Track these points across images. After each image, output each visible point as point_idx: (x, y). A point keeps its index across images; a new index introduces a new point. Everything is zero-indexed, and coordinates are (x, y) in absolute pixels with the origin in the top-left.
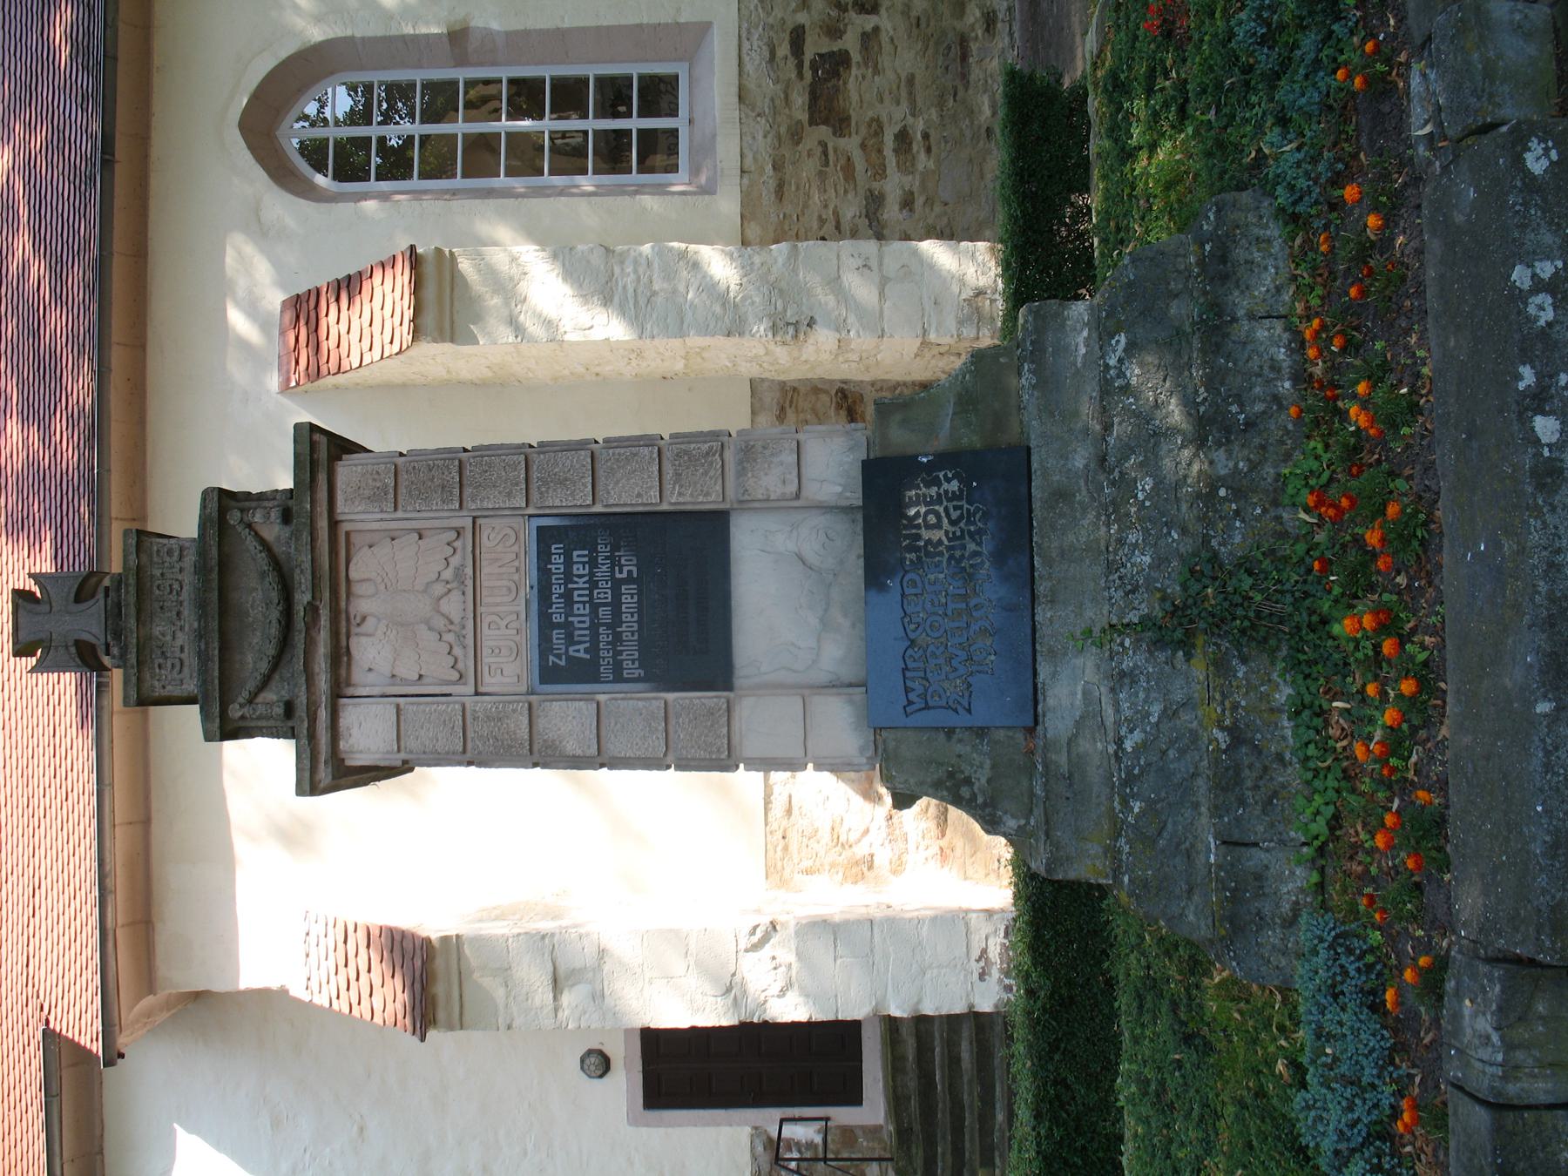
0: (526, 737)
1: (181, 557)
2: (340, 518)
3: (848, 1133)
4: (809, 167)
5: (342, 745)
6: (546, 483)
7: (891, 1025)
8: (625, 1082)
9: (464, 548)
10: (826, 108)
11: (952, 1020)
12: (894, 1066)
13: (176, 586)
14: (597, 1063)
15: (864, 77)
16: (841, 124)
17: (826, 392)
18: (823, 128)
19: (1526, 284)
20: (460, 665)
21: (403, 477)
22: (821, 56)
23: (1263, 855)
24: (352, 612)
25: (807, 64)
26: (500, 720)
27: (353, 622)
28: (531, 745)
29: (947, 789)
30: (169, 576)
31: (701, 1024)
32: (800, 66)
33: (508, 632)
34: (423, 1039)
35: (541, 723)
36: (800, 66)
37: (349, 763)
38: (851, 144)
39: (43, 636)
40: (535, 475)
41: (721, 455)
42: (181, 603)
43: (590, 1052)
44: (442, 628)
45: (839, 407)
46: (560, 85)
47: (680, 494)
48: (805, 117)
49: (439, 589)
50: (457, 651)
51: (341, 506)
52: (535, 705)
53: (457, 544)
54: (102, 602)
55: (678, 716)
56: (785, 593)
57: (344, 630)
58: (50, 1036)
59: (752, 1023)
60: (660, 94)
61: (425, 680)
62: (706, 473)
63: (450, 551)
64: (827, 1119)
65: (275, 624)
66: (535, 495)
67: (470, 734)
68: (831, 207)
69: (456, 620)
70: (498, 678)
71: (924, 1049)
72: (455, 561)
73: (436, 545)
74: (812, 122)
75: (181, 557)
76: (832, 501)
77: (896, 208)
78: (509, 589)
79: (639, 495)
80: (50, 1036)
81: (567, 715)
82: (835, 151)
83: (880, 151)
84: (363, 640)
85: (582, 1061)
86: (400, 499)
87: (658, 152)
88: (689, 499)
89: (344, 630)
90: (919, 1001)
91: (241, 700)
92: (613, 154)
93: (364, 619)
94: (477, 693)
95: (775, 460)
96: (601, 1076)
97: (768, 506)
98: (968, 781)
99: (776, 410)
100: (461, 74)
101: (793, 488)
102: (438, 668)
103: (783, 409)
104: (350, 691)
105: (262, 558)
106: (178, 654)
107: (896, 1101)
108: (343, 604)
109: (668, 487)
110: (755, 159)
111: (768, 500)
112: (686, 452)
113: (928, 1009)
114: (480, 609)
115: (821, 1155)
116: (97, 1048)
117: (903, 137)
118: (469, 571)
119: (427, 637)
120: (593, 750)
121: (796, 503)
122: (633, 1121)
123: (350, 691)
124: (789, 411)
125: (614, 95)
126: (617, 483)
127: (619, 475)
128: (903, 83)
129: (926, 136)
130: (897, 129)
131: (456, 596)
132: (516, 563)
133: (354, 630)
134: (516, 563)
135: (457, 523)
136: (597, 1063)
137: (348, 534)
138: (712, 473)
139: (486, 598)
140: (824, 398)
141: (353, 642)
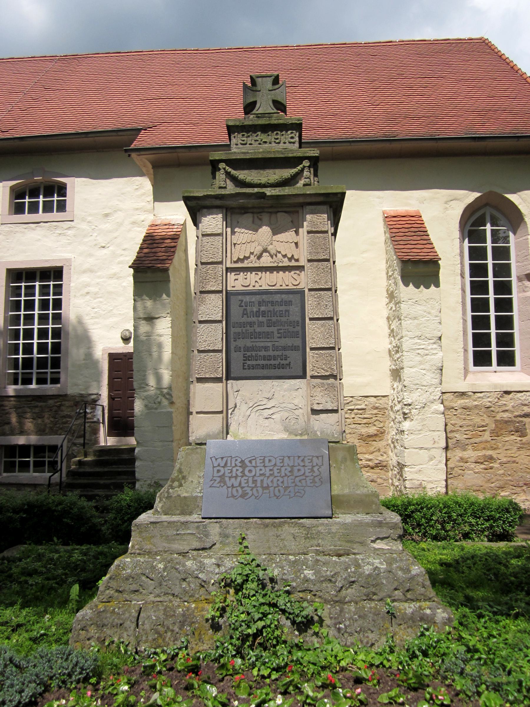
1: (290, 143)
3: (96, 431)
4: (477, 420)
10: (503, 427)
11: (133, 473)
13: (277, 141)
15: (516, 442)
16: (496, 433)
18: (494, 426)
22: (525, 425)
23: (132, 628)
24: (263, 214)
25: (521, 419)
29: (178, 476)
30: (282, 137)
32: (520, 416)
34: (130, 267)
35: (213, 296)
36: (520, 416)
37: (198, 214)
38: (487, 436)
39: (258, 88)
42: (270, 143)
46: (510, 319)
48: (498, 418)
54: (273, 111)
58: (138, 131)
60: (507, 359)
68: (461, 429)
74: (496, 421)
75: (290, 143)
77: (460, 455)
80: (138, 131)
82: (484, 431)
83: (484, 449)
84: (251, 219)
85: (128, 330)
87: (481, 359)
90: (141, 460)
91: (227, 168)
92: (480, 340)
93: (260, 219)
94: (227, 269)
98: (181, 485)
100: (514, 279)
104: (229, 214)
106: (249, 143)
108: (266, 210)
110: (479, 397)
113: (137, 463)
115: (87, 421)
116: (132, 146)
117: (491, 459)
123: (229, 214)
125: (506, 340)
128: (514, 459)
129: (491, 468)
130: (495, 456)
132: (284, 285)
133: (255, 216)
134: (284, 285)
137: (298, 212)
141: (250, 215)
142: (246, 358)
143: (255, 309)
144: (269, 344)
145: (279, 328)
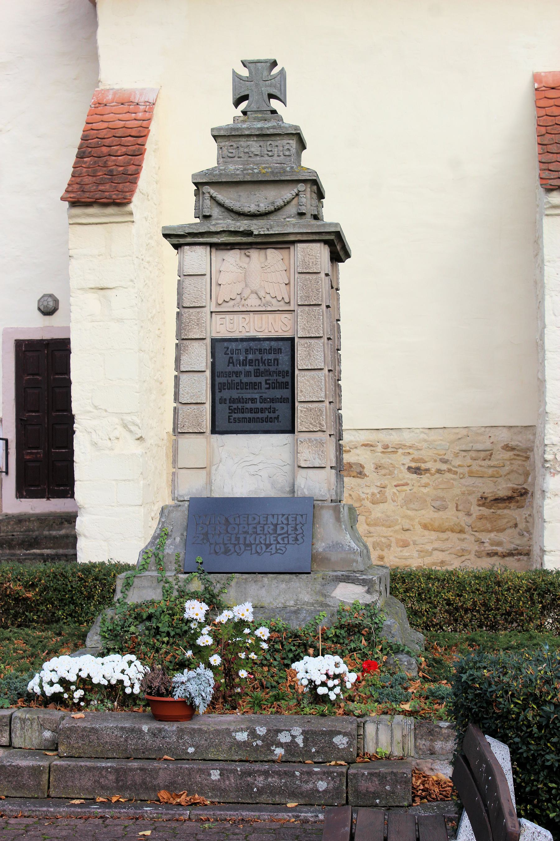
0: (190, 337)
2: (296, 245)
5: (187, 248)
6: (309, 346)
7: (70, 519)
8: (37, 327)
9: (281, 306)
12: (44, 520)
14: (49, 309)
17: (525, 481)
19: (294, 733)
20: (225, 304)
21: (314, 276)
26: (198, 325)
27: (247, 251)
28: (186, 339)
31: (73, 387)
33: (241, 327)
35: (196, 344)
40: (312, 341)
41: (320, 431)
43: (56, 301)
44: (242, 295)
45: (514, 490)
47: (301, 411)
49: (262, 294)
50: (232, 303)
51: (300, 246)
52: (204, 341)
53: (282, 303)
55: (198, 409)
56: (250, 466)
57: (242, 247)
59: (74, 423)
61: (218, 287)
62: (311, 424)
63: (280, 299)
64: (7, 473)
65: (249, 209)
66: (303, 341)
67: (191, 310)
69: (246, 302)
70: (219, 322)
71: (56, 541)
72: (274, 301)
73: (282, 292)
76: (297, 483)
78: (261, 327)
79: (302, 391)
81: (200, 357)
85: (51, 296)
86: (303, 276)
88: (299, 415)
89: (242, 247)
93: (248, 256)
94: (211, 312)
95: (317, 456)
96: (39, 309)
97: (295, 453)
99: (513, 444)
101: (303, 465)
102: (224, 294)
103: (513, 449)
105: (280, 203)
107: (20, 519)
109: (305, 405)
111: (298, 453)
112: (321, 414)
114: (251, 314)
118: (269, 309)
119: (239, 288)
120: (183, 369)
121: (296, 466)
122: (6, 332)
124: (511, 453)
126: (308, 381)
127: (312, 382)
131: (258, 302)
132: (273, 331)
133: (243, 251)
135: (292, 303)
136: (49, 309)
137: (289, 248)
138: (311, 426)
139: (257, 316)
140: (521, 479)
142: (232, 411)
143: (241, 358)
144: (257, 396)
145: (267, 378)
